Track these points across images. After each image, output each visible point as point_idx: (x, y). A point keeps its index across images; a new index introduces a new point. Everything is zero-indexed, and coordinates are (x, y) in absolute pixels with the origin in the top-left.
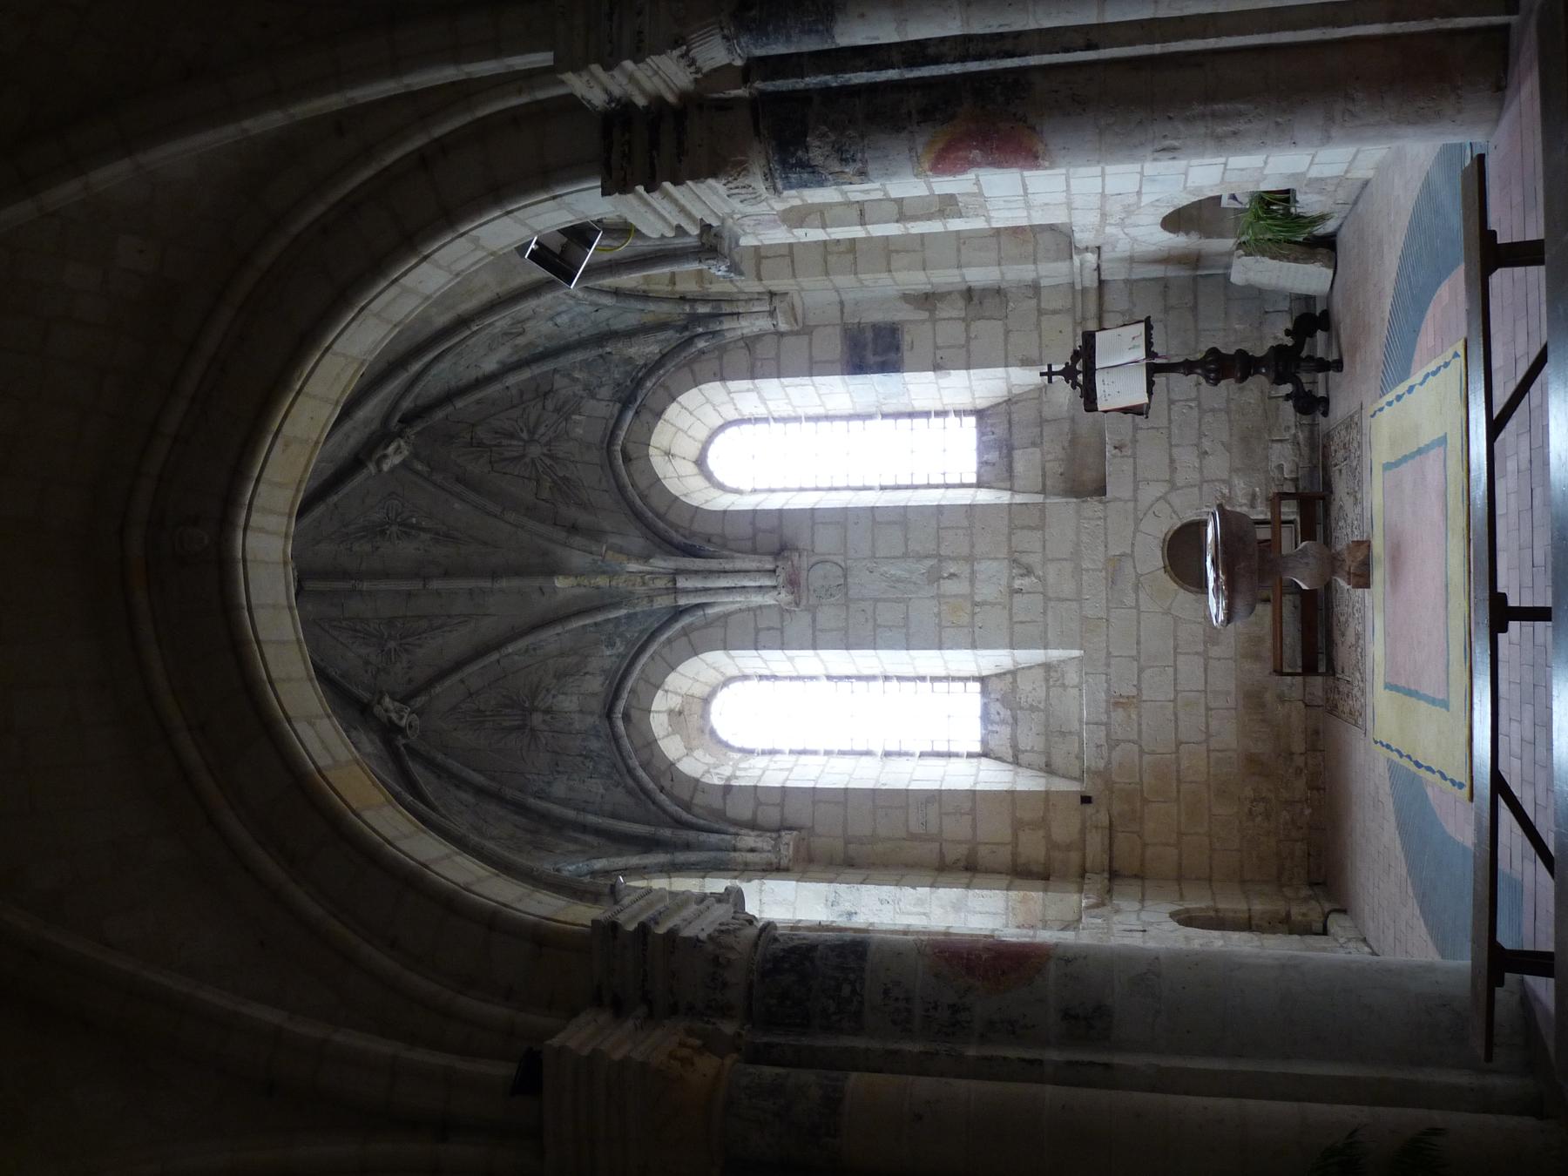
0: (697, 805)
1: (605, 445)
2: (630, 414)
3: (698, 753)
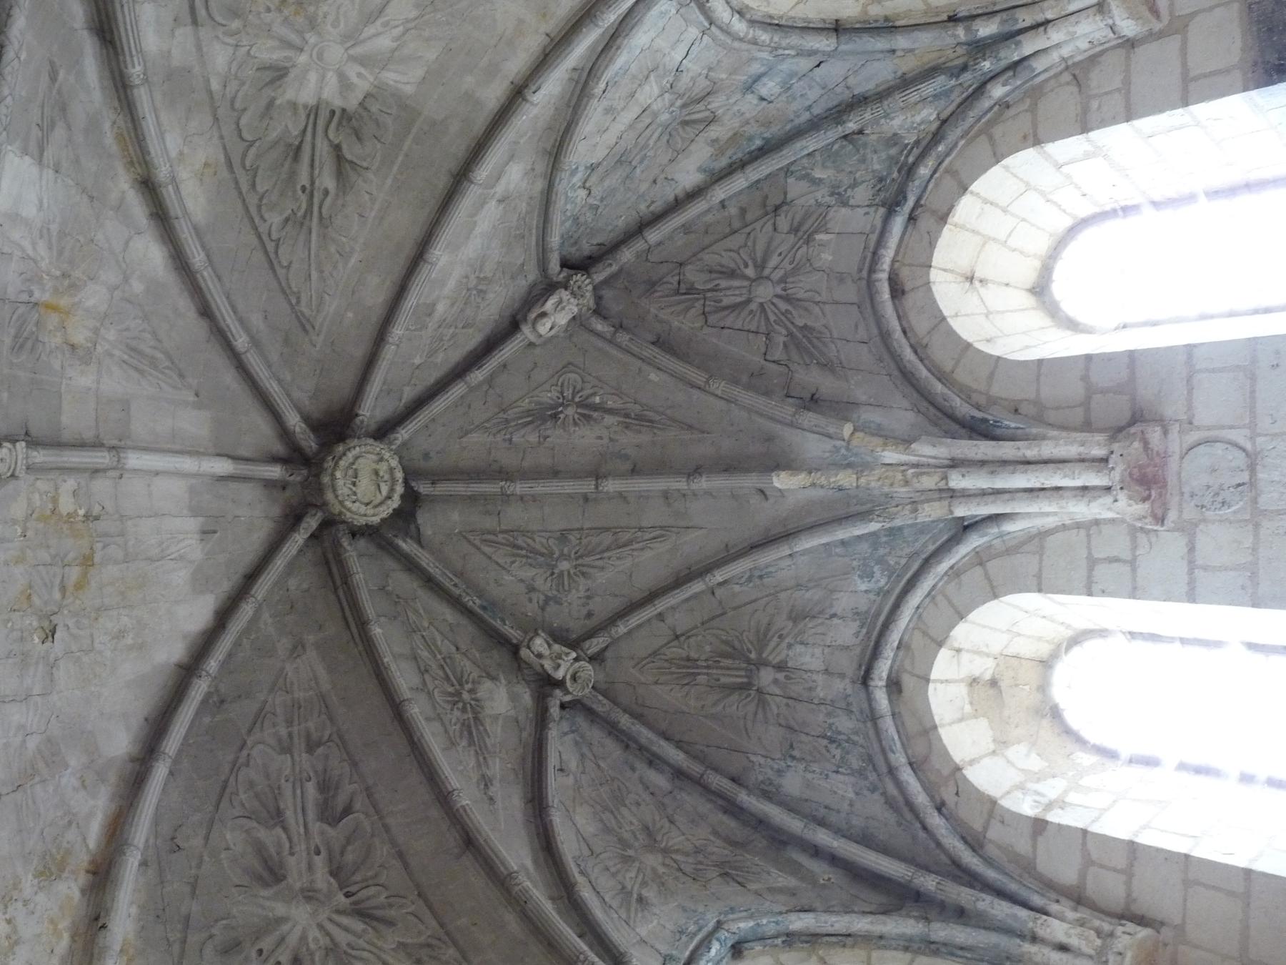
0: (990, 841)
1: (865, 274)
2: (898, 223)
3: (1017, 753)
